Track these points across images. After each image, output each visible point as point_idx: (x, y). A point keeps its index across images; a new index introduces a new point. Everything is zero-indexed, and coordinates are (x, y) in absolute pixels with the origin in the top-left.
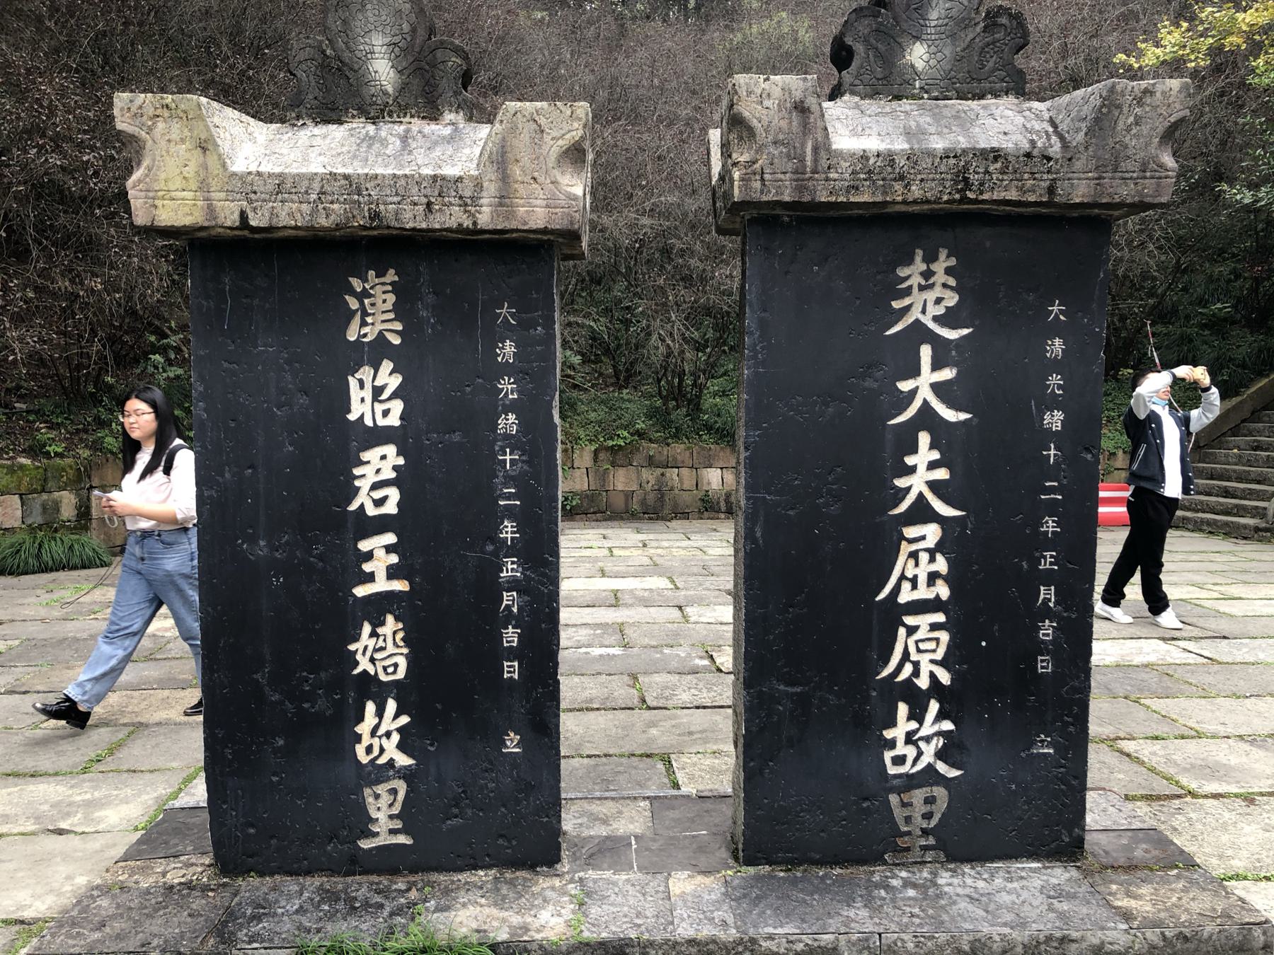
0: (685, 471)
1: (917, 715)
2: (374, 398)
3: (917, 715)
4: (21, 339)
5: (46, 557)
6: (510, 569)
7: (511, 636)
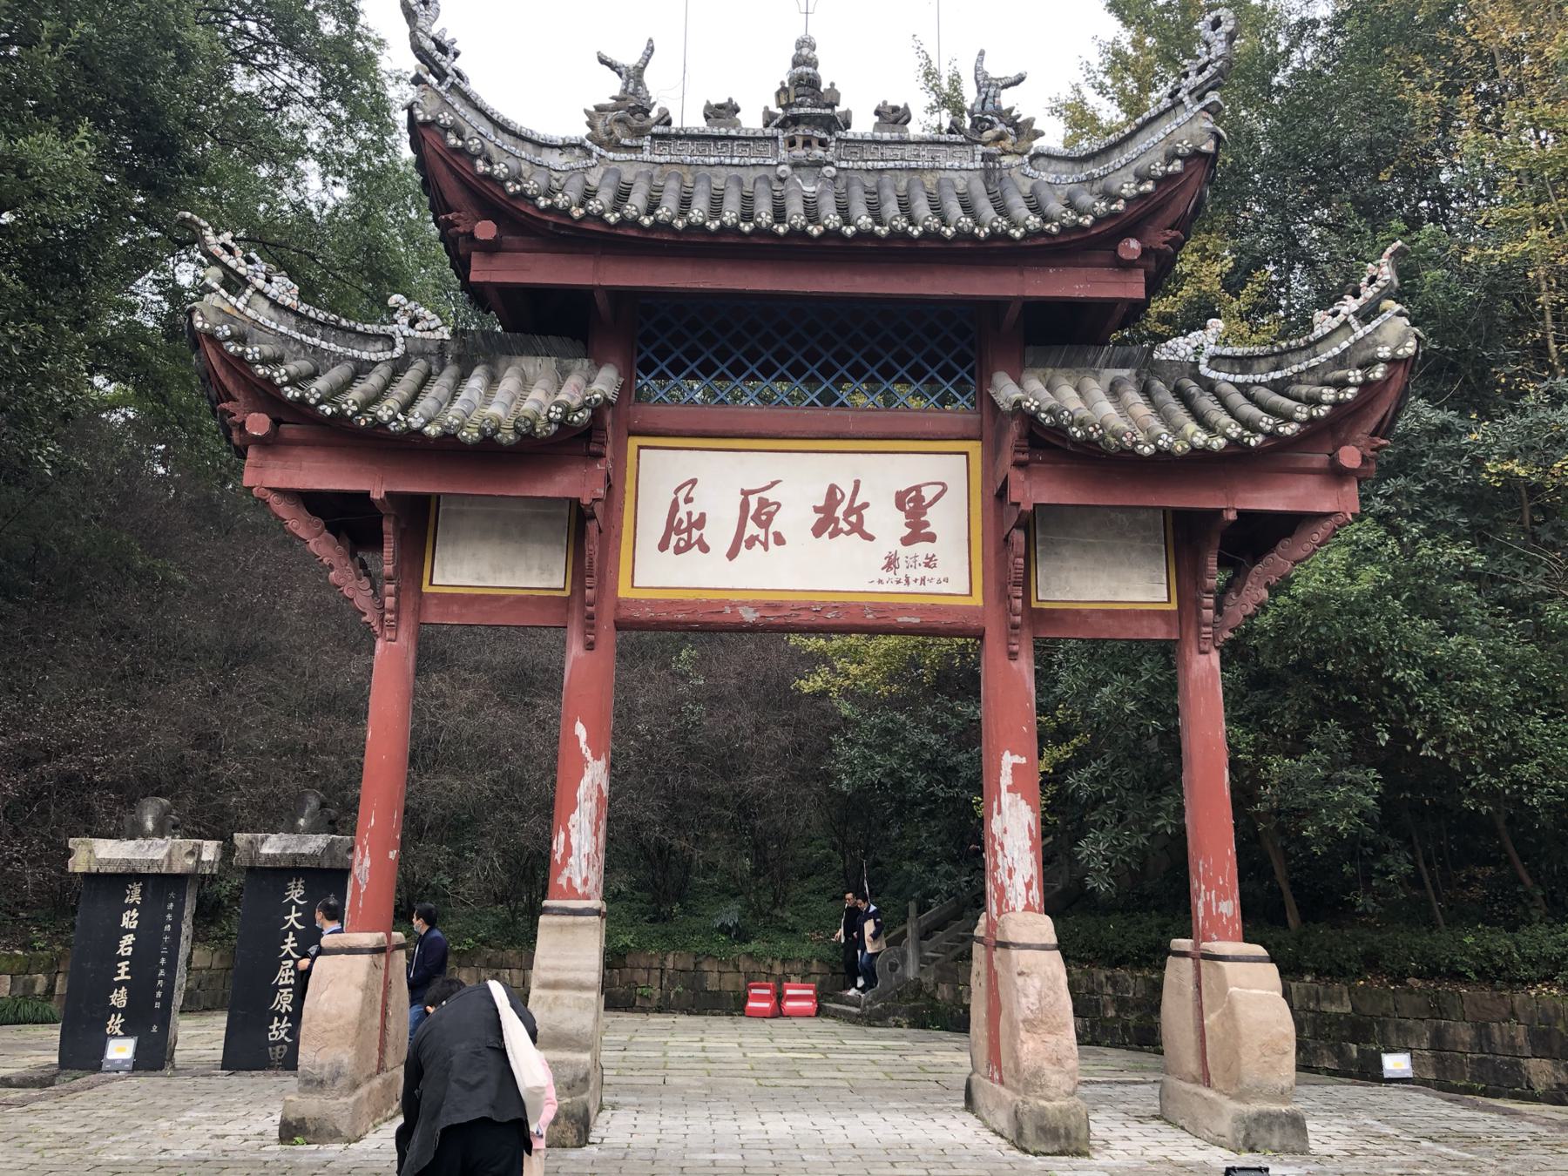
0: (515, 972)
1: (280, 1021)
2: (129, 920)
3: (280, 1021)
4: (33, 874)
5: (20, 1014)
6: (162, 973)
7: (159, 994)
